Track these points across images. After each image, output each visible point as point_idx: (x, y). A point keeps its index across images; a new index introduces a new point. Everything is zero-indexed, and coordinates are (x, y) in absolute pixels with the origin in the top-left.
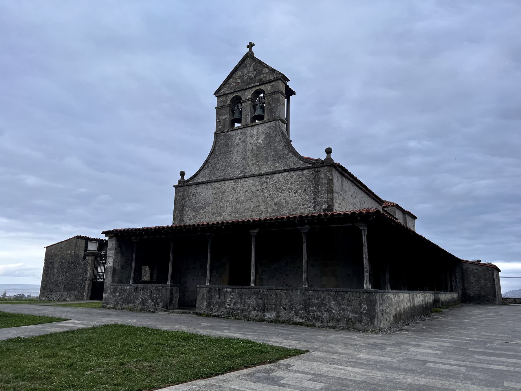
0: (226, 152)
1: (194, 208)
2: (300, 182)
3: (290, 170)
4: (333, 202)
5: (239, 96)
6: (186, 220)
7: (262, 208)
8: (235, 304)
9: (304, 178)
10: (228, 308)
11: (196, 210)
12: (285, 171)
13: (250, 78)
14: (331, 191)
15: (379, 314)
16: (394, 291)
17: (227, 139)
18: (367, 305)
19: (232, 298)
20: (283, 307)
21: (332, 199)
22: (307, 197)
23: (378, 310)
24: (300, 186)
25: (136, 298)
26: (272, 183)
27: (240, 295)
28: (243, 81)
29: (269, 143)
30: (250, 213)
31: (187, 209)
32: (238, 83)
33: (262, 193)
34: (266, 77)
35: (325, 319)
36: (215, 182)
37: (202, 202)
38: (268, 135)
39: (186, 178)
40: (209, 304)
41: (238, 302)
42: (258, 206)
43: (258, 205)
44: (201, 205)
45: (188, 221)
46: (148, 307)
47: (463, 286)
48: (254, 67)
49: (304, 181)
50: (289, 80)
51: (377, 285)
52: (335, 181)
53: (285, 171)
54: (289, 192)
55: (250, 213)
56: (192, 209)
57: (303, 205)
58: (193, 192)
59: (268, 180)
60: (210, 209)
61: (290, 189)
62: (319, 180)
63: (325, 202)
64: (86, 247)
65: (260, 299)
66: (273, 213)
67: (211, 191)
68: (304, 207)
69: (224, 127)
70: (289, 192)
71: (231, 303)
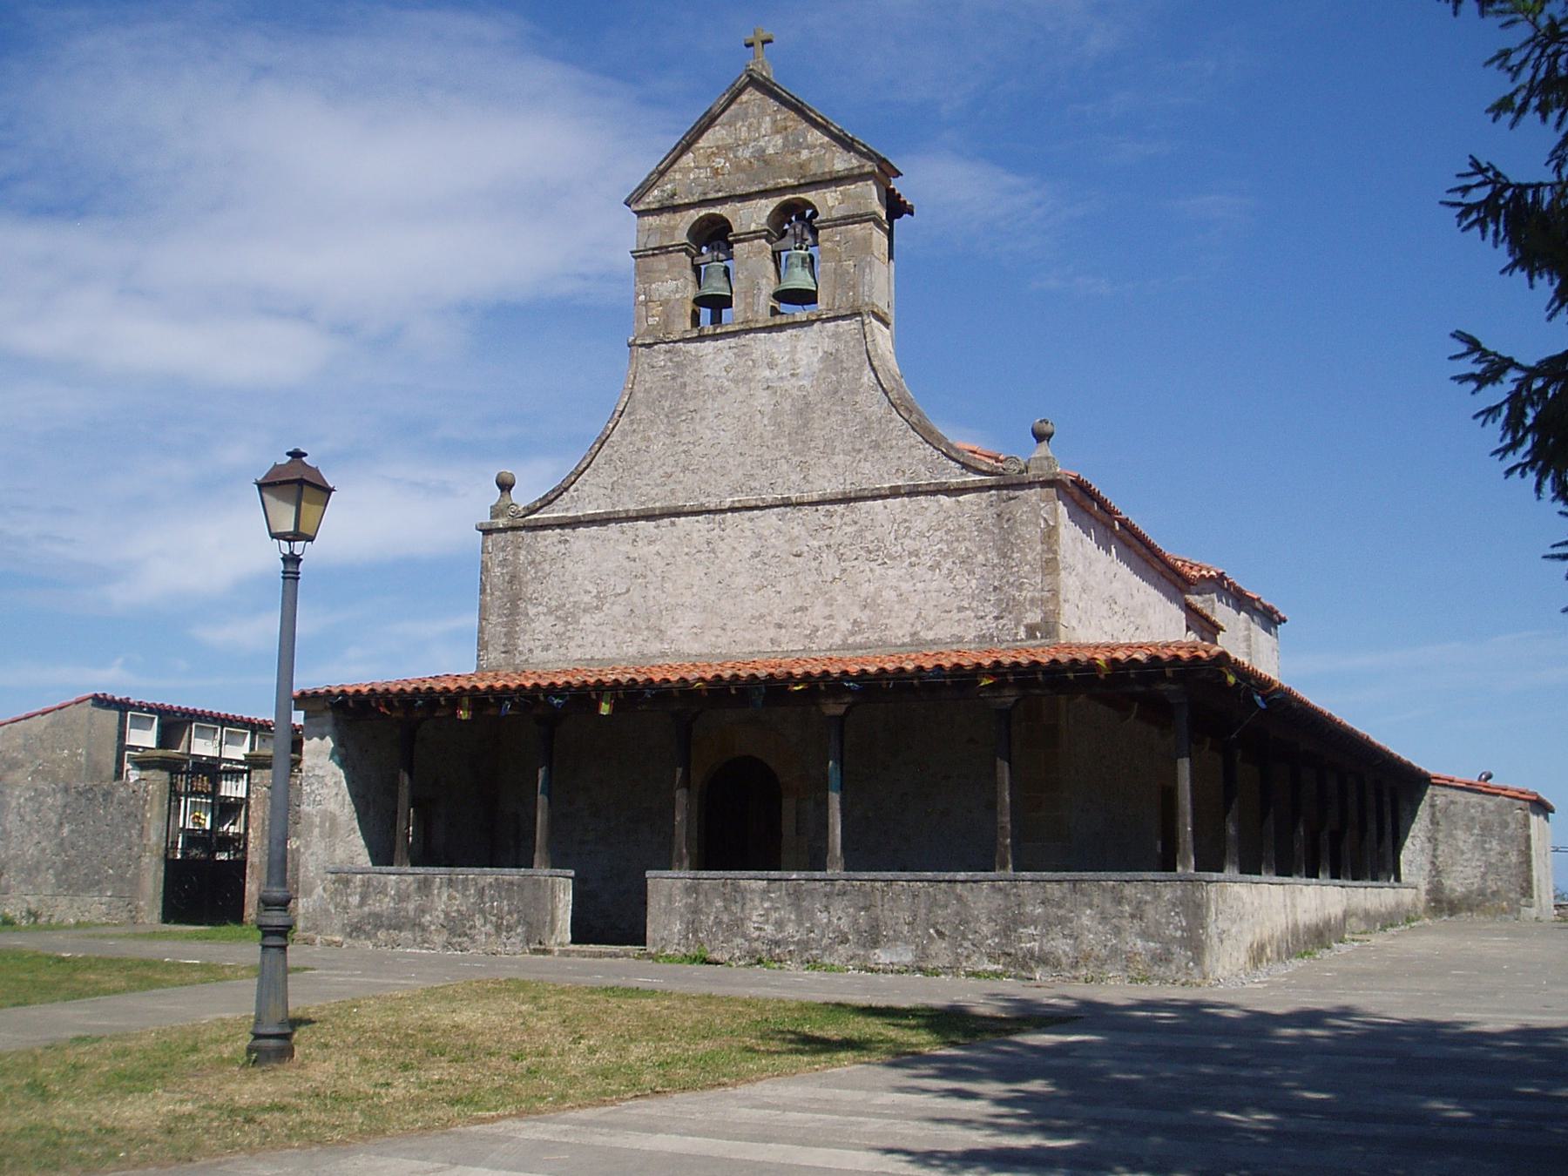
0: (673, 413)
1: (558, 608)
2: (948, 532)
3: (913, 492)
4: (1058, 604)
5: (721, 217)
6: (531, 651)
7: (818, 611)
8: (780, 925)
9: (964, 521)
10: (757, 940)
11: (566, 616)
12: (895, 493)
13: (760, 154)
14: (1050, 565)
15: (1215, 939)
16: (1248, 877)
17: (679, 366)
18: (1186, 916)
19: (767, 910)
20: (937, 931)
21: (1055, 593)
22: (974, 583)
23: (1212, 930)
24: (949, 543)
25: (422, 911)
26: (848, 529)
27: (796, 897)
28: (738, 168)
29: (836, 392)
30: (772, 632)
31: (532, 611)
32: (716, 172)
33: (814, 564)
34: (819, 159)
35: (1064, 960)
36: (637, 519)
37: (590, 587)
38: (832, 360)
39: (522, 497)
40: (693, 927)
41: (789, 920)
42: (802, 609)
43: (799, 603)
44: (587, 598)
45: (537, 652)
46: (766, 915)
47: (1433, 863)
48: (774, 122)
49: (961, 528)
50: (899, 174)
51: (1210, 861)
52: (1062, 530)
53: (895, 493)
54: (912, 565)
55: (772, 632)
56: (550, 612)
57: (961, 609)
58: (552, 551)
59: (837, 520)
60: (619, 610)
61: (915, 553)
62: (1011, 530)
63: (1032, 601)
64: (122, 735)
65: (862, 909)
66: (853, 634)
67: (623, 548)
68: (962, 615)
69: (667, 322)
70: (912, 565)
71: (767, 922)
